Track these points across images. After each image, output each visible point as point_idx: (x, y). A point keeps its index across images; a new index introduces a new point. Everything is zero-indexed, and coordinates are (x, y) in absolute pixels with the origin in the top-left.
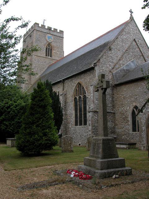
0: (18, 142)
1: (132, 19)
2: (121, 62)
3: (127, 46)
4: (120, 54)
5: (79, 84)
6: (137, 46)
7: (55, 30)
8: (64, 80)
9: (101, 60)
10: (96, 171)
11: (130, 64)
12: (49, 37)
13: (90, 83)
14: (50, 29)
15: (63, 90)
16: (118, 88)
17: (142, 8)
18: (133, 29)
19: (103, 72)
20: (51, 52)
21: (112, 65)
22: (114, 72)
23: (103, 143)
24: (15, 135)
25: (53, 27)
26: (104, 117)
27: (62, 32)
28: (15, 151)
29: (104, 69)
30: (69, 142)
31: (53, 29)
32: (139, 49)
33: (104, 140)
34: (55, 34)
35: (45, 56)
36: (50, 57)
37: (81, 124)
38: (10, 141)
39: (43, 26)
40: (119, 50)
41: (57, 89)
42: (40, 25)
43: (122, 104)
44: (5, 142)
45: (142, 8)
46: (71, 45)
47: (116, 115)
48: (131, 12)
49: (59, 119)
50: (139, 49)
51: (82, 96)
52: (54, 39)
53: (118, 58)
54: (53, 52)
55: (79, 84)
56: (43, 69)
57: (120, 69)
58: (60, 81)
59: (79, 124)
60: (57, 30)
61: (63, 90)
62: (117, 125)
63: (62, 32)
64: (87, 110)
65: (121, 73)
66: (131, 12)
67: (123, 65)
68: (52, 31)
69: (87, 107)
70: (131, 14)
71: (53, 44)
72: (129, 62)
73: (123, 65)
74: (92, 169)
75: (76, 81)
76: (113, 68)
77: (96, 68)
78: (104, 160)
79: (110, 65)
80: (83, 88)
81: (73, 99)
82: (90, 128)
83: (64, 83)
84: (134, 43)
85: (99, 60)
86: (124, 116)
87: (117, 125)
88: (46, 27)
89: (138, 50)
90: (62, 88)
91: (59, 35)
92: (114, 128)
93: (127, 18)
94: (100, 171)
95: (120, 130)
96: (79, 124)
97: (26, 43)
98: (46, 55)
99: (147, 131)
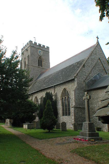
1: (98, 42)
2: (91, 75)
3: (95, 63)
4: (90, 69)
6: (101, 63)
7: (44, 46)
9: (79, 74)
10: (87, 137)
11: (96, 76)
12: (40, 52)
13: (72, 88)
14: (40, 45)
15: (54, 92)
17: (106, 44)
18: (98, 51)
19: (80, 82)
20: (42, 63)
21: (85, 77)
22: (87, 81)
24: (8, 120)
25: (42, 44)
26: (88, 117)
27: (48, 48)
29: (80, 80)
32: (102, 65)
34: (43, 49)
35: (38, 66)
36: (41, 67)
37: (66, 115)
39: (35, 43)
40: (89, 67)
42: (33, 43)
43: (92, 103)
44: (22, 127)
45: (106, 44)
46: (56, 59)
48: (98, 38)
49: (56, 113)
50: (102, 65)
51: (67, 97)
53: (89, 72)
54: (43, 63)
55: (65, 89)
57: (89, 80)
59: (65, 115)
60: (44, 46)
63: (48, 48)
64: (70, 106)
65: (91, 82)
66: (98, 38)
67: (92, 76)
68: (42, 47)
69: (70, 104)
70: (98, 39)
71: (43, 57)
72: (96, 74)
73: (92, 76)
74: (85, 137)
75: (63, 87)
77: (76, 79)
79: (84, 77)
80: (67, 92)
81: (61, 99)
82: (73, 117)
83: (54, 88)
84: (99, 61)
85: (77, 74)
86: (93, 111)
88: (38, 44)
89: (102, 65)
90: (54, 91)
91: (46, 50)
93: (94, 43)
94: (88, 138)
96: (65, 115)
98: (39, 66)
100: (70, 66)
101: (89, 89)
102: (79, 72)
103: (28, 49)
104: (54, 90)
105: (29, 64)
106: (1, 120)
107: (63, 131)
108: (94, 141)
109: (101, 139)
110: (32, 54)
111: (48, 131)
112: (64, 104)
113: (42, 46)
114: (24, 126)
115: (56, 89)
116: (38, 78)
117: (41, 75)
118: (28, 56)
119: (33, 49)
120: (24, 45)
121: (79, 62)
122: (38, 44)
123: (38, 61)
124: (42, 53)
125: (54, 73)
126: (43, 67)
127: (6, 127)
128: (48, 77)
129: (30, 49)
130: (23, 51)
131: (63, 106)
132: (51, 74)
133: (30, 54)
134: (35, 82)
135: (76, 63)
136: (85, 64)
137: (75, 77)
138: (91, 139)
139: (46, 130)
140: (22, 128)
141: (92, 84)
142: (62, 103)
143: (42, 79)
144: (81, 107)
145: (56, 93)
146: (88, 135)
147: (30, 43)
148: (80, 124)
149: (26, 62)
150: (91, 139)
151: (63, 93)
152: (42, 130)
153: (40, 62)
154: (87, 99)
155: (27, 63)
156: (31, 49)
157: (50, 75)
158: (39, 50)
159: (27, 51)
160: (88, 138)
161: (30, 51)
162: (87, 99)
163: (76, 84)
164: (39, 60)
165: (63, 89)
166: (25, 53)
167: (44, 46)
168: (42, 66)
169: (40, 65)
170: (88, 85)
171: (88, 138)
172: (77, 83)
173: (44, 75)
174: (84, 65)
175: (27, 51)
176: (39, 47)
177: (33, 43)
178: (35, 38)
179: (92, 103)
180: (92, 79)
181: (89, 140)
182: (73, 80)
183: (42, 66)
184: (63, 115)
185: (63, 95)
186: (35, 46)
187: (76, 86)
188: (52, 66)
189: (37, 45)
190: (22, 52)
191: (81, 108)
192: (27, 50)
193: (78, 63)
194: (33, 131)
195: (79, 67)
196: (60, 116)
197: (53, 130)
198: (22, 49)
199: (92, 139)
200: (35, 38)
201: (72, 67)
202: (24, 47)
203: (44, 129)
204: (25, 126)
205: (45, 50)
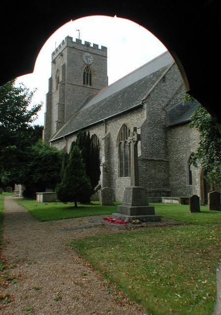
0: (11, 297)
2: (178, 96)
5: (125, 126)
7: (96, 46)
8: (106, 120)
9: (152, 95)
12: (87, 57)
14: (87, 44)
15: (106, 132)
16: (173, 130)
20: (90, 78)
21: (166, 100)
22: (169, 109)
23: (134, 192)
27: (104, 49)
28: (56, 196)
30: (110, 195)
31: (92, 45)
33: (134, 189)
34: (95, 51)
36: (89, 86)
38: (42, 196)
39: (79, 41)
41: (99, 133)
42: (74, 40)
43: (177, 151)
44: (35, 198)
47: (170, 164)
52: (94, 59)
54: (93, 78)
55: (124, 126)
56: (81, 102)
58: (102, 122)
59: (124, 174)
60: (97, 46)
61: (106, 132)
62: (171, 176)
63: (104, 49)
68: (91, 47)
71: (93, 67)
74: (123, 216)
75: (121, 122)
76: (167, 105)
77: (145, 105)
78: (133, 207)
79: (163, 101)
81: (118, 144)
85: (149, 95)
86: (179, 166)
87: (171, 176)
88: (83, 43)
92: (168, 179)
95: (175, 183)
97: (57, 65)
98: (84, 83)
99: (201, 183)
100: (140, 81)
101: (172, 124)
102: (153, 91)
103: (64, 52)
104: (106, 128)
105: (65, 80)
106: (7, 187)
107: (105, 205)
108: (139, 223)
109: (158, 219)
110: (71, 61)
111: (74, 205)
112: (124, 154)
113: (92, 45)
114: (38, 196)
115: (109, 127)
116: (82, 107)
117: (88, 101)
118: (64, 66)
119: (73, 51)
120: (57, 46)
121: (156, 72)
122: (83, 43)
123: (84, 75)
124: (91, 60)
125: (111, 96)
126: (94, 86)
127: (11, 202)
128: (99, 103)
129: (68, 53)
130: (55, 56)
131: (120, 157)
132: (105, 99)
133: (66, 62)
134: (76, 116)
135: (151, 75)
136: (167, 76)
137: (144, 102)
138: (134, 219)
139: (70, 204)
140: (34, 201)
141: (180, 113)
142: (120, 152)
143: (88, 109)
144: (155, 158)
145: (109, 134)
146: (129, 211)
147: (68, 42)
148: (150, 192)
149: (59, 77)
150: (134, 219)
151: (120, 134)
152: (60, 205)
153: (87, 78)
154: (134, 141)
155: (61, 79)
156: (69, 53)
157: (102, 101)
158: (86, 53)
159: (62, 56)
160: (127, 217)
161: (68, 56)
162: (134, 141)
163: (145, 115)
164: (84, 73)
165: (122, 125)
166: (58, 61)
167: (97, 46)
168: (90, 85)
169: (87, 82)
170: (172, 116)
171: (127, 217)
172: (148, 114)
173: (92, 100)
174: (164, 77)
175: (62, 56)
176: (85, 47)
177: (74, 40)
178: (79, 30)
179: (177, 151)
180: (181, 106)
181: (130, 221)
182: (139, 108)
183: (90, 85)
184: (121, 175)
185: (122, 137)
186: (77, 46)
187: (145, 118)
188: (111, 82)
189: (83, 45)
190: (52, 58)
191: (154, 160)
192: (61, 55)
193: (154, 74)
194: (51, 205)
195: (153, 83)
196: (114, 178)
197: (92, 204)
198: (53, 54)
199: (137, 218)
200: (79, 30)
201: (143, 83)
202: (57, 50)
203: (64, 200)
204: (40, 197)
205: (99, 54)
